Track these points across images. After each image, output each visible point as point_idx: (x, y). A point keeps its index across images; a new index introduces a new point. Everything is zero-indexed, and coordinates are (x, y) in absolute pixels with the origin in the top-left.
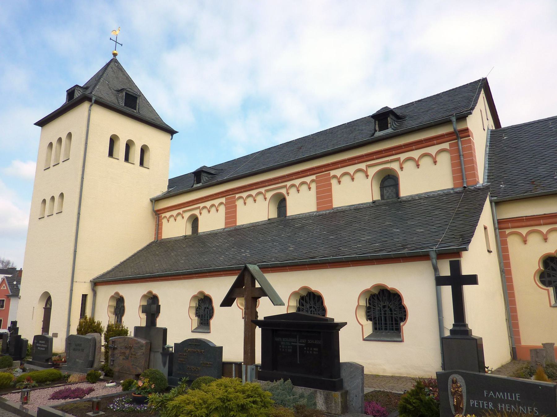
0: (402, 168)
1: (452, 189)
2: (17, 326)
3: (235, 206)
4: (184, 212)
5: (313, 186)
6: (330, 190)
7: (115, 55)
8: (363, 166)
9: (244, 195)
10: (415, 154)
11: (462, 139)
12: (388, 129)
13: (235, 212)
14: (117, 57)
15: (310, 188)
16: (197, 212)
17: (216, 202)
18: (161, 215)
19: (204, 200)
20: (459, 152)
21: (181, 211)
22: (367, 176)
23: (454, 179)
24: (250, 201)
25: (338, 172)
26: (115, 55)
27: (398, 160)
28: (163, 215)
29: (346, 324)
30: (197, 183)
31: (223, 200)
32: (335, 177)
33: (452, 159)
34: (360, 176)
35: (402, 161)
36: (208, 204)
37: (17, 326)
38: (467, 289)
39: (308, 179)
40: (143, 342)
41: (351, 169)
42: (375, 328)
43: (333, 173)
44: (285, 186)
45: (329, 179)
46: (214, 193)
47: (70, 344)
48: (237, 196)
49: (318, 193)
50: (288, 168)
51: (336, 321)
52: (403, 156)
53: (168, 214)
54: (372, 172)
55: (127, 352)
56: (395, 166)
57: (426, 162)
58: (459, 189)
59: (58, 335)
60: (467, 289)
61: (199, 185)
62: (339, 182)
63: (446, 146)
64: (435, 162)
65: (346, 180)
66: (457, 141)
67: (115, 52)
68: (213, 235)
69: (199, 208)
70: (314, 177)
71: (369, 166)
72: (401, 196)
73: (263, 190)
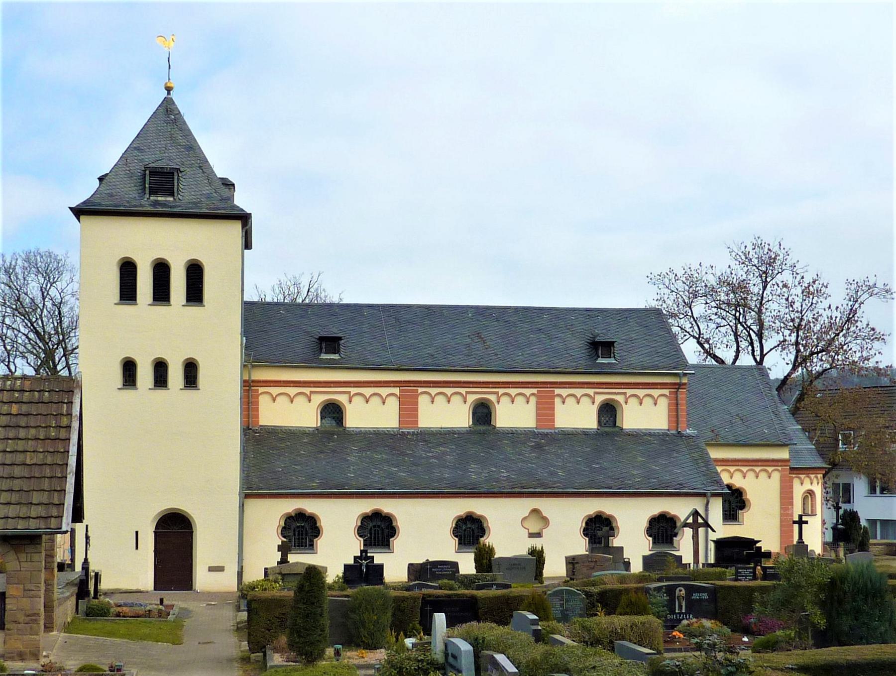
0: (626, 403)
1: (668, 430)
2: (280, 553)
3: (417, 403)
4: (467, 393)
5: (533, 400)
6: (553, 409)
7: (169, 89)
8: (591, 392)
9: (433, 391)
10: (641, 392)
11: (253, 388)
12: (610, 357)
13: (416, 410)
14: (174, 95)
15: (528, 402)
16: (342, 399)
17: (384, 391)
18: (257, 388)
19: (500, 386)
20: (677, 400)
21: (307, 390)
22: (465, 402)
23: (670, 422)
24: (440, 400)
25: (564, 392)
26: (169, 89)
27: (625, 394)
28: (261, 390)
29: (760, 541)
30: (326, 353)
31: (396, 391)
32: (559, 395)
33: (669, 405)
34: (585, 401)
35: (352, 394)
36: (368, 391)
37: (280, 553)
38: (804, 525)
39: (528, 392)
40: (611, 556)
41: (579, 392)
42: (654, 543)
43: (557, 391)
44: (497, 393)
45: (553, 397)
46: (264, 379)
47: (775, 587)
48: (420, 390)
49: (538, 409)
50: (502, 375)
51: (755, 539)
52: (630, 392)
53: (275, 391)
54: (471, 398)
55: (593, 564)
56: (620, 399)
57: (648, 401)
58: (674, 432)
59: (225, 568)
60: (804, 525)
61: (332, 356)
62: (564, 402)
63: (666, 392)
64: (641, 404)
65: (571, 401)
66: (248, 388)
67: (169, 85)
68: (514, 436)
69: (349, 393)
70: (535, 391)
71: (596, 393)
72: (347, 426)
73: (463, 391)
